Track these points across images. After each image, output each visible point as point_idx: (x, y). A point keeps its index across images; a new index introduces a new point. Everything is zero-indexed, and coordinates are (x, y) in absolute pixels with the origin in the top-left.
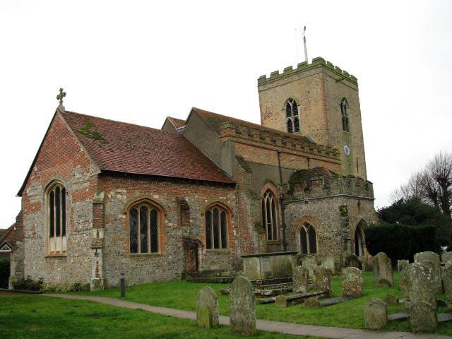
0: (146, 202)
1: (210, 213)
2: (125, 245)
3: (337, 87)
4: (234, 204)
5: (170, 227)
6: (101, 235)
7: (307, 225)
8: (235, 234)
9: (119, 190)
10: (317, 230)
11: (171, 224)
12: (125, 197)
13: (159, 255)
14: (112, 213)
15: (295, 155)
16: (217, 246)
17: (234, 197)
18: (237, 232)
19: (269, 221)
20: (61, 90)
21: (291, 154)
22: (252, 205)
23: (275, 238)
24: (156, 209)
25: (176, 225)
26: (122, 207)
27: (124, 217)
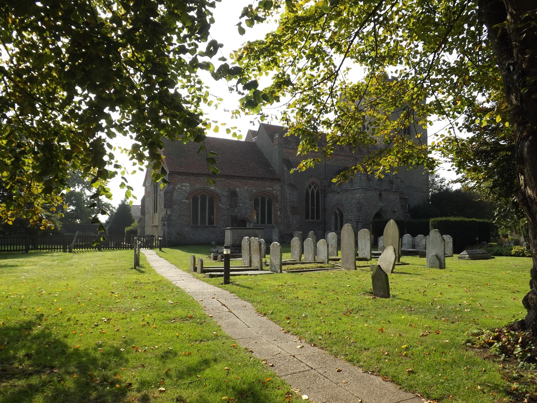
0: (204, 192)
1: (198, 197)
4: (279, 193)
5: (223, 208)
7: (339, 209)
8: (279, 214)
9: (184, 184)
10: (344, 214)
11: (223, 207)
12: (188, 188)
13: (214, 227)
14: (178, 198)
15: (343, 155)
16: (313, 218)
17: (279, 188)
18: (281, 213)
19: (313, 205)
23: (318, 218)
24: (213, 198)
26: (186, 195)
27: (187, 201)
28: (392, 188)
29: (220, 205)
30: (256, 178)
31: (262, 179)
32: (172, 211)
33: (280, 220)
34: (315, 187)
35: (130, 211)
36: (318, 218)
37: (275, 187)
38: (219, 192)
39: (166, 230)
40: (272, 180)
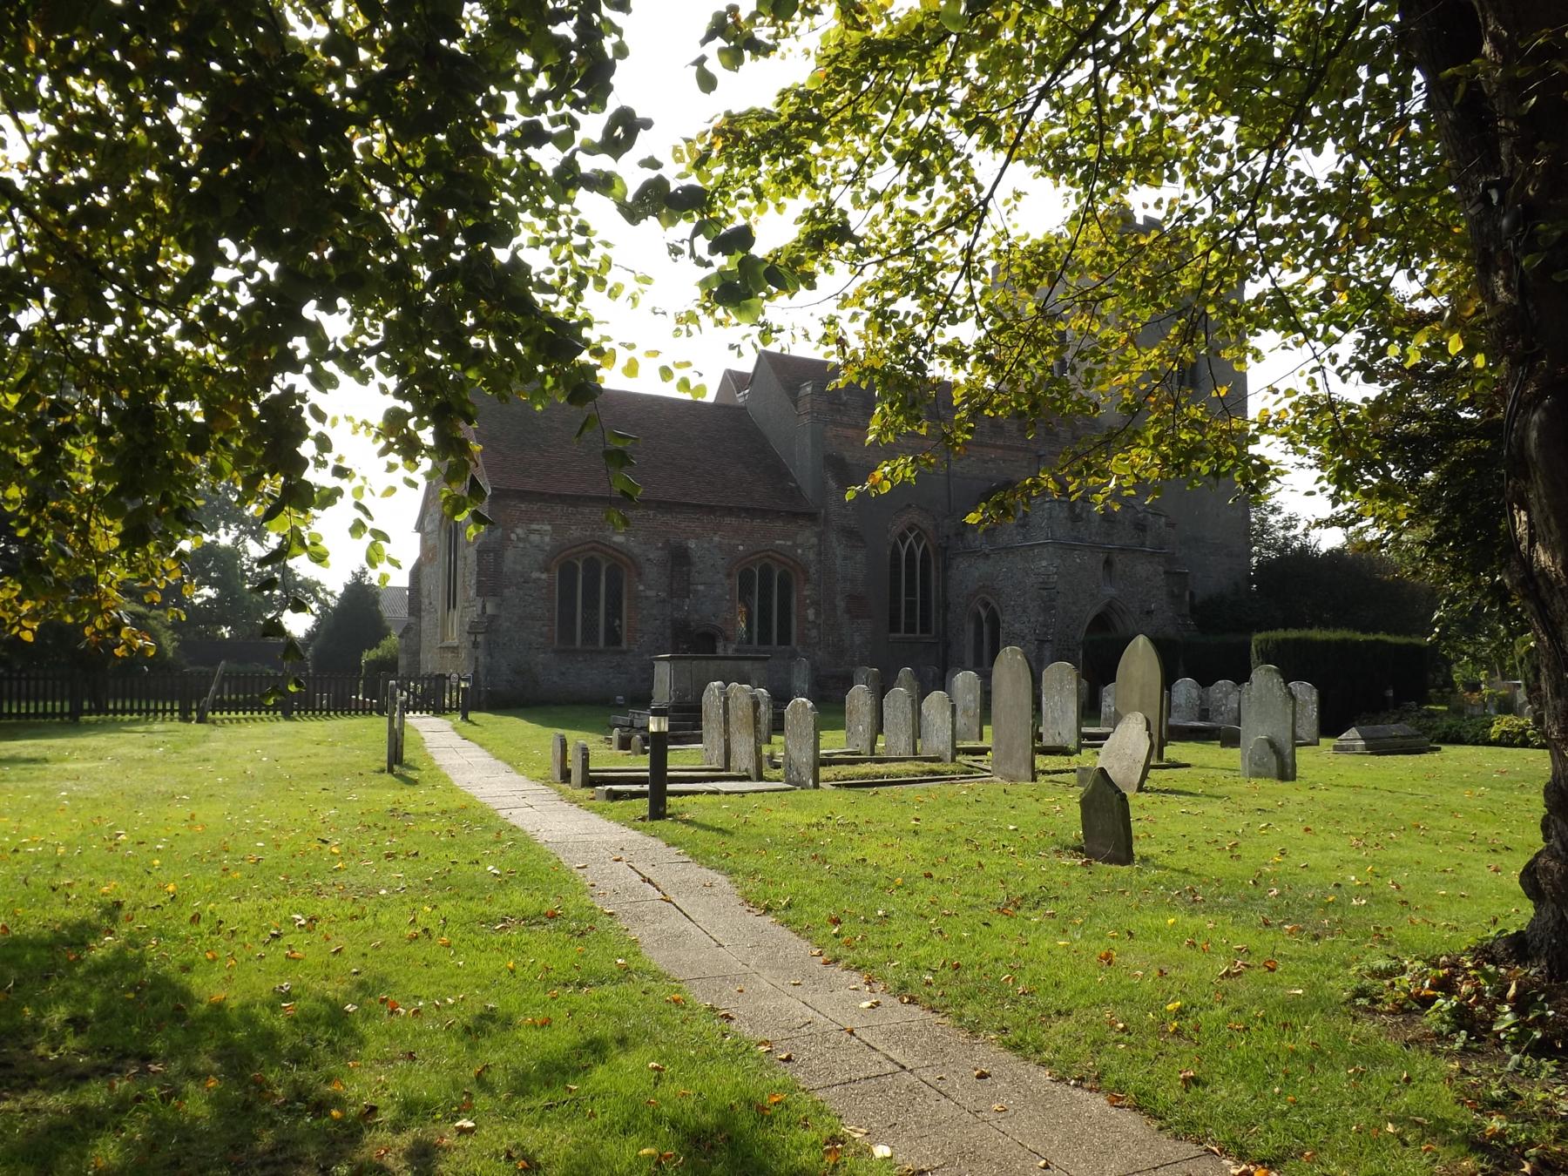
0: (593, 549)
1: (576, 567)
2: (545, 629)
3: (327, 566)
4: (811, 556)
5: (647, 598)
6: (489, 610)
7: (986, 605)
8: (811, 617)
9: (534, 527)
10: (1001, 618)
11: (649, 593)
12: (547, 539)
13: (624, 653)
14: (519, 568)
17: (814, 540)
18: (817, 614)
20: (647, 124)
21: (987, 446)
22: (845, 558)
23: (925, 628)
24: (620, 567)
25: (663, 595)
27: (544, 576)
28: (1143, 545)
29: (641, 588)
30: (747, 510)
31: (764, 513)
32: (498, 606)
33: (814, 633)
34: (918, 538)
35: (376, 602)
36: (925, 628)
37: (800, 539)
38: (636, 551)
39: (481, 659)
40: (794, 516)
